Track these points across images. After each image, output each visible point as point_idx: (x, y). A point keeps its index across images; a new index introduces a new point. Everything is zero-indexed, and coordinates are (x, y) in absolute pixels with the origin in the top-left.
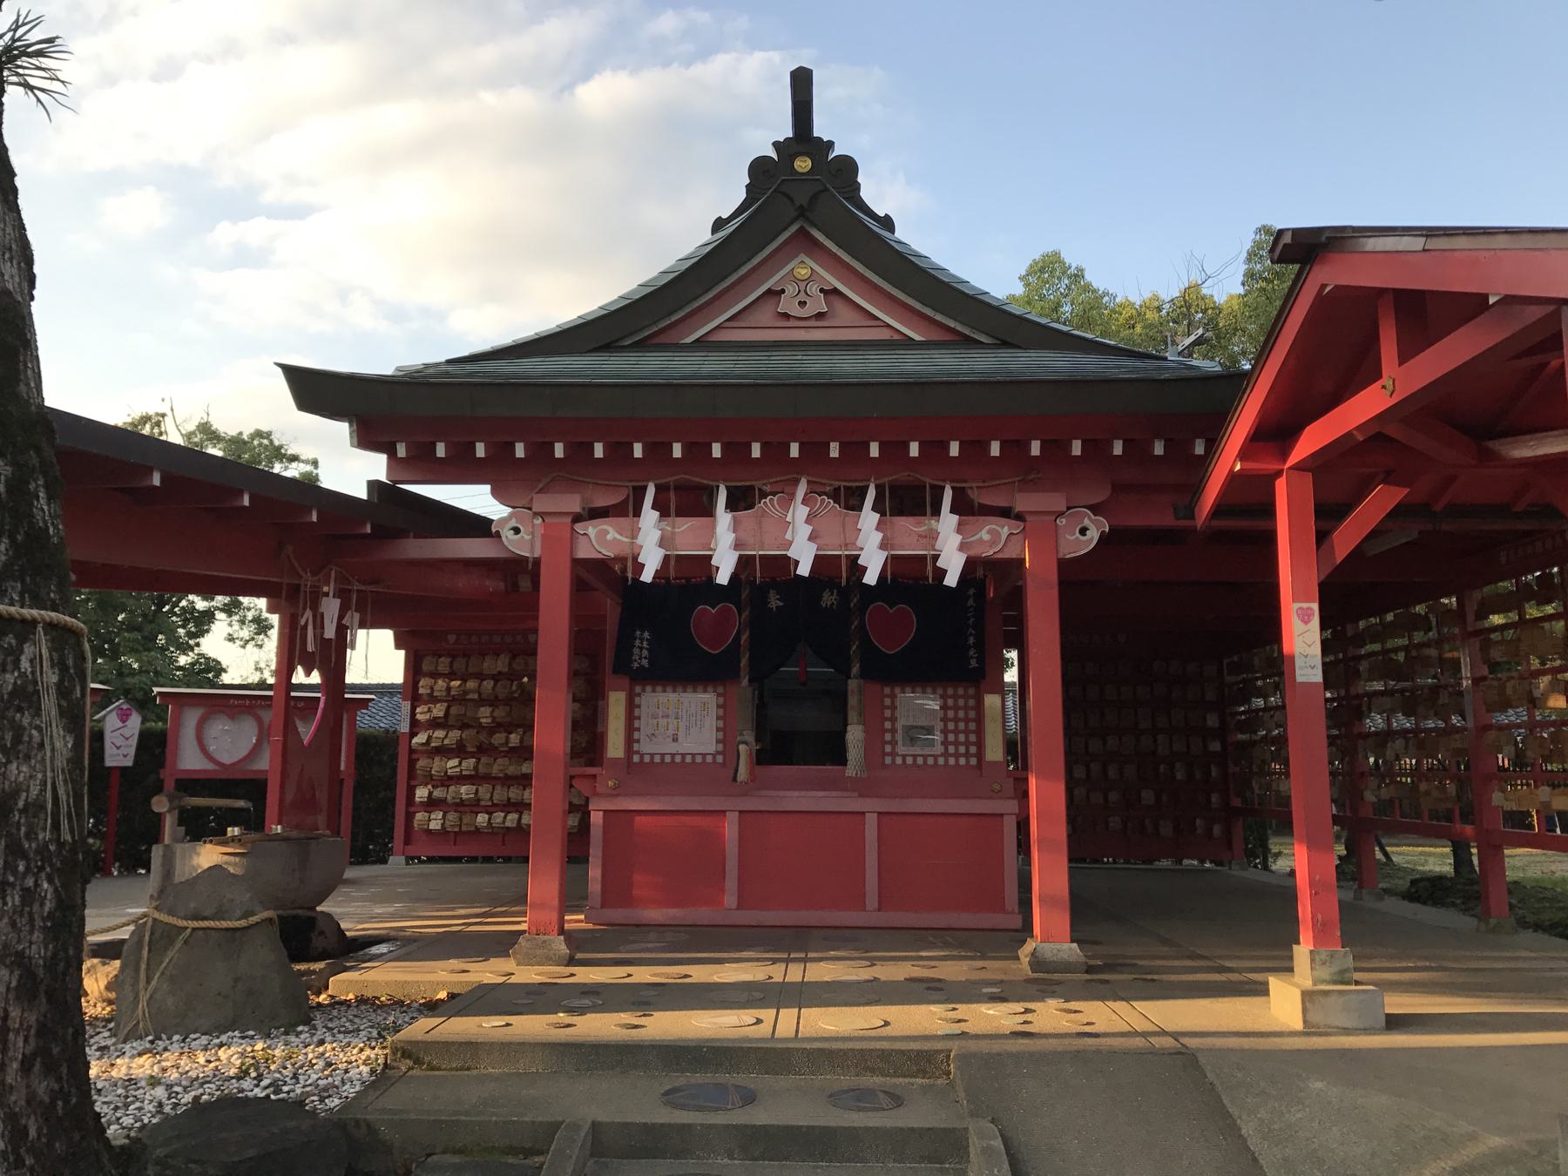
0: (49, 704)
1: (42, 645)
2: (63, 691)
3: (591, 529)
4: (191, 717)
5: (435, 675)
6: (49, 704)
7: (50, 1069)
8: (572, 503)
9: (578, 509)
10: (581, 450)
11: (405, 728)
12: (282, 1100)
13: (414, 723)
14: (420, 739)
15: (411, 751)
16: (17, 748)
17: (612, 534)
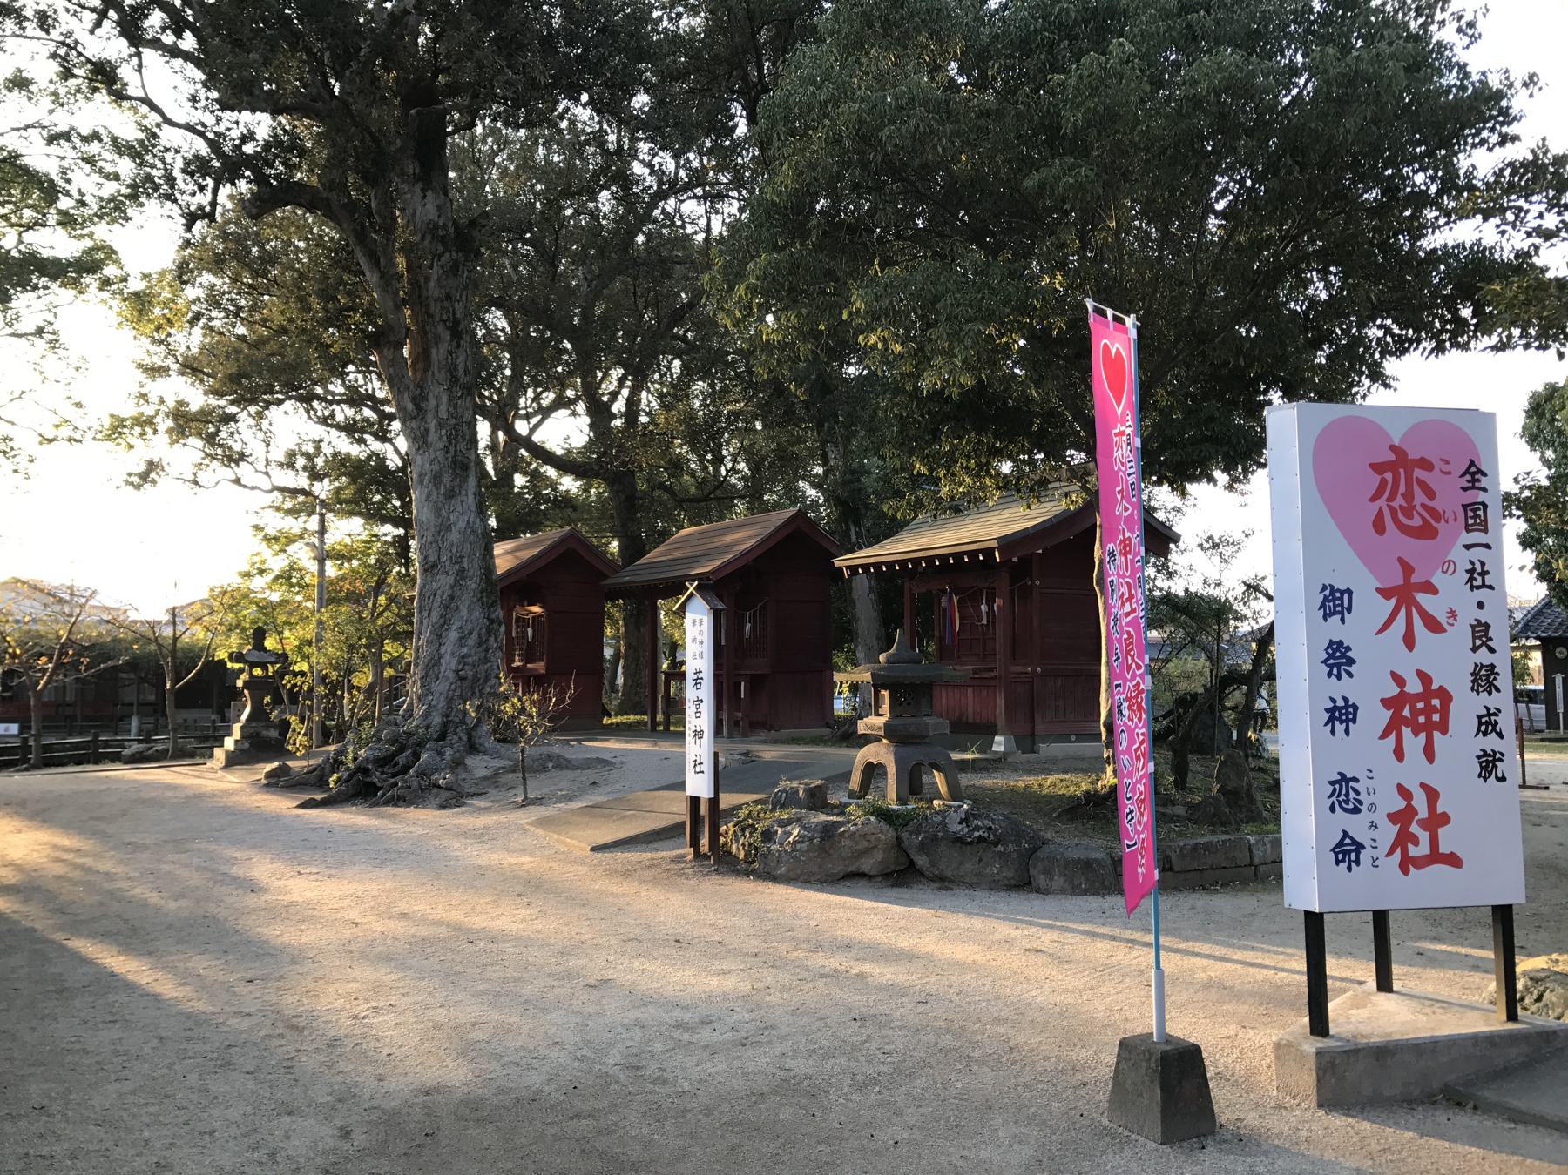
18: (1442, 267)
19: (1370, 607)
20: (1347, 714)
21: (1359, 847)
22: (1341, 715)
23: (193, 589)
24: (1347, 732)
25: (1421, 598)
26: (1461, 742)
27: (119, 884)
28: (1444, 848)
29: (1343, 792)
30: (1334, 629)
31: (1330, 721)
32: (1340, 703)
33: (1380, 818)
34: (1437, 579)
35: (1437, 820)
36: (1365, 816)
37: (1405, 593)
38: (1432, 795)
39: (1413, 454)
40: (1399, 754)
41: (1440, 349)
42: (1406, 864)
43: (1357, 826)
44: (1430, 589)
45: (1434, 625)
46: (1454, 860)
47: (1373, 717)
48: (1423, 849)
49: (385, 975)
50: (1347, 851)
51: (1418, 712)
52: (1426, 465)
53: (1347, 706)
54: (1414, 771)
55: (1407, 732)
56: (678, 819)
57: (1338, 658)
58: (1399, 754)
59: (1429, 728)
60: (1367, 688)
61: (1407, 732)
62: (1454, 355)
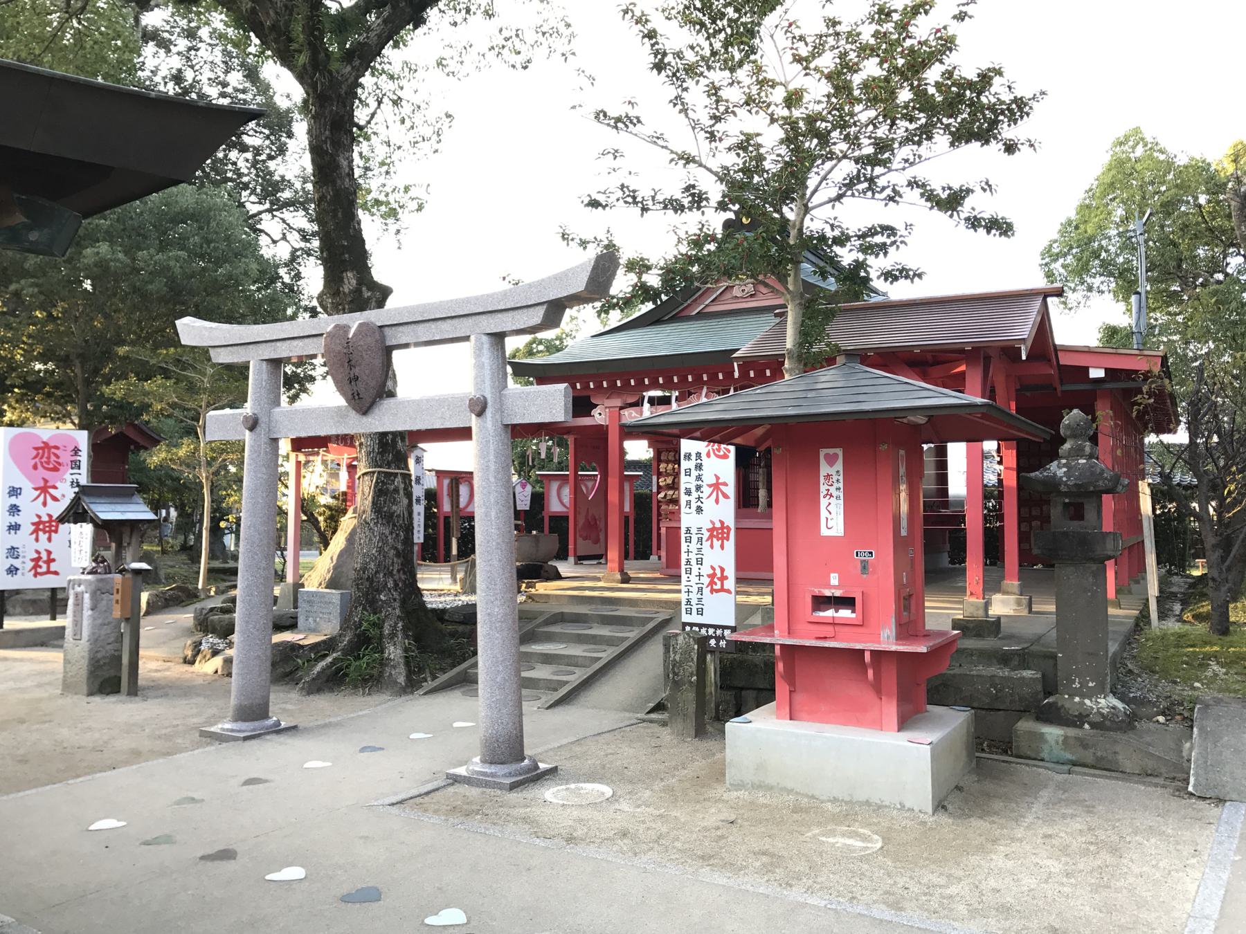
0: (401, 492)
1: (399, 479)
2: (405, 489)
3: (626, 412)
4: (554, 486)
5: (668, 462)
6: (401, 492)
7: (405, 573)
8: (618, 402)
9: (620, 405)
10: (612, 385)
11: (655, 490)
12: (62, 435)
13: (659, 487)
14: (662, 495)
15: (659, 502)
16: (395, 502)
17: (634, 414)
19: (29, 492)
20: (723, 533)
21: (17, 569)
24: (722, 547)
25: (52, 491)
28: (52, 569)
30: (13, 500)
31: (36, 531)
32: (718, 525)
33: (27, 560)
34: (58, 484)
35: (50, 561)
36: (21, 559)
37: (44, 488)
38: (49, 553)
39: (52, 444)
40: (37, 540)
42: (36, 575)
43: (17, 563)
44: (55, 487)
46: (56, 573)
47: (27, 528)
48: (44, 569)
52: (57, 448)
53: (723, 527)
54: (43, 544)
55: (41, 533)
56: (149, 618)
58: (37, 540)
59: (722, 539)
61: (41, 533)
62: (1059, 227)
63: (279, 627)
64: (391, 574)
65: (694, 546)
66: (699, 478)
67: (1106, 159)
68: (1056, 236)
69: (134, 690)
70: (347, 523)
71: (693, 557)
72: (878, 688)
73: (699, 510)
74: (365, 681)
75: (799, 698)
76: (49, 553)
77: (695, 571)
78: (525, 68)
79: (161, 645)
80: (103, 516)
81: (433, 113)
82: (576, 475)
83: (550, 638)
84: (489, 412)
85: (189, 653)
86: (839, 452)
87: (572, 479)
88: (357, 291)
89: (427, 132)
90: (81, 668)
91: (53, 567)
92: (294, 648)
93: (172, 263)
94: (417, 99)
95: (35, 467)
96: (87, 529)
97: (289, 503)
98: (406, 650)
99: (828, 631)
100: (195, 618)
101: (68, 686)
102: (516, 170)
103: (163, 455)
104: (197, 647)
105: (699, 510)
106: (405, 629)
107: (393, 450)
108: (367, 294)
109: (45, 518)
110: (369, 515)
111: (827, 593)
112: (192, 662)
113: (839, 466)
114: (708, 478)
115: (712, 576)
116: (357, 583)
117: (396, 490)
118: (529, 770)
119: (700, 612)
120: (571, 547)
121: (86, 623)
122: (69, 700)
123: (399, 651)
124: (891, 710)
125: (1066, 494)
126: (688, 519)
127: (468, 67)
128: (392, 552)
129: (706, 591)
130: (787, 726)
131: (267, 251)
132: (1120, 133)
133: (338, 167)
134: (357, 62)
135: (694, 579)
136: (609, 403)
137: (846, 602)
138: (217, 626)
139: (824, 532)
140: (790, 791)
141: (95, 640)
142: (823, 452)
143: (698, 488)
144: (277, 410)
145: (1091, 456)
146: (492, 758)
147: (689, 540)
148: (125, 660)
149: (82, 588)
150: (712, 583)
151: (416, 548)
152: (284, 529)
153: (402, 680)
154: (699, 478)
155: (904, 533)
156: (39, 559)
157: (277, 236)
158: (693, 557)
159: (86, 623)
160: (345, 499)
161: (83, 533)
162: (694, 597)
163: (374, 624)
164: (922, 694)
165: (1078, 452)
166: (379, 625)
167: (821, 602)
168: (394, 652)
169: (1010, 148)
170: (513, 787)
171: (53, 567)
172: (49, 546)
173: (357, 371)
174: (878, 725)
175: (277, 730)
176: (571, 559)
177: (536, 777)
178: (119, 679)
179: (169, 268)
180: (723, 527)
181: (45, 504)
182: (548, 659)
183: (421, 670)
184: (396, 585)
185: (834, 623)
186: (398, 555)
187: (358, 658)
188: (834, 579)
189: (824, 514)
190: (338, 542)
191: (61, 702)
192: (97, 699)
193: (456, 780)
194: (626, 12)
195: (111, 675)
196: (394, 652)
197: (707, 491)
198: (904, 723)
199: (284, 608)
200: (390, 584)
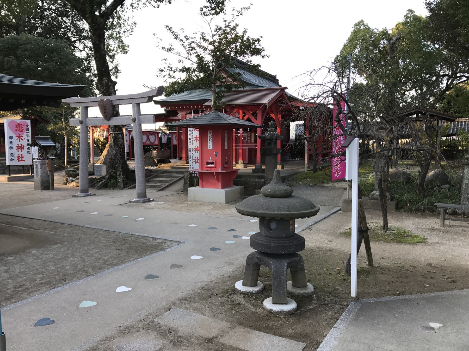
1: (120, 135)
8: (185, 113)
18: (252, 49)
19: (15, 138)
22: (11, 148)
23: (350, 34)
26: (25, 150)
27: (183, 205)
29: (12, 155)
30: (11, 140)
31: (18, 149)
35: (22, 157)
37: (19, 137)
41: (344, 45)
43: (13, 158)
45: (22, 140)
46: (24, 161)
47: (15, 148)
48: (21, 159)
49: (345, 264)
50: (12, 160)
51: (21, 148)
53: (22, 146)
54: (20, 152)
57: (11, 143)
60: (15, 145)
63: (90, 175)
64: (119, 160)
65: (191, 152)
66: (192, 136)
67: (352, 30)
68: (339, 54)
69: (53, 189)
70: (107, 146)
71: (191, 155)
72: (217, 179)
73: (193, 144)
74: (112, 187)
75: (204, 183)
76: (22, 155)
77: (192, 157)
78: (158, 7)
79: (58, 177)
80: (42, 145)
81: (130, 22)
82: (179, 132)
83: (162, 177)
84: (136, 121)
85: (65, 182)
86: (212, 131)
87: (177, 133)
88: (107, 83)
89: (128, 28)
90: (39, 183)
91: (23, 159)
92: (94, 179)
93: (50, 67)
94: (125, 18)
95: (16, 131)
96: (37, 148)
97: (91, 141)
98: (123, 179)
99: (209, 169)
100: (66, 173)
101: (35, 188)
102: (149, 55)
103: (52, 127)
104: (67, 180)
105: (193, 144)
106: (123, 174)
107: (118, 129)
108: (110, 84)
109: (20, 145)
110: (112, 145)
111: (209, 161)
112: (66, 184)
113: (212, 134)
114: (195, 136)
115: (195, 159)
116: (110, 162)
117: (119, 138)
118: (147, 199)
119: (193, 168)
120: (177, 154)
121: (39, 172)
122: (37, 192)
123: (121, 179)
124: (220, 184)
125: (268, 140)
126: (190, 146)
127: (141, 6)
128: (119, 154)
129: (194, 163)
130: (201, 189)
131: (78, 54)
132: (357, 22)
133: (101, 48)
134: (105, 18)
135: (191, 160)
136: (182, 113)
137: (212, 163)
138: (73, 175)
139: (209, 148)
140: (200, 201)
141: (42, 176)
142: (209, 131)
143: (192, 138)
144: (87, 119)
145: (274, 131)
146: (139, 197)
147: (190, 151)
148: (50, 181)
149: (38, 163)
150: (195, 161)
151: (126, 154)
152: (90, 149)
153: (122, 186)
154: (192, 136)
155: (226, 148)
156: (19, 157)
157: (82, 49)
158: (191, 155)
159: (39, 172)
160: (107, 139)
161: (35, 150)
162: (191, 164)
163: (114, 173)
164: (232, 182)
165: (271, 131)
166: (116, 173)
167: (208, 163)
168: (120, 179)
169: (263, 57)
170: (143, 202)
171: (23, 159)
172: (22, 153)
173: (106, 111)
174: (218, 188)
175: (91, 195)
176: (178, 158)
177: (149, 201)
178: (49, 186)
179: (49, 68)
180: (22, 146)
181: (20, 141)
182: (160, 181)
183: (127, 184)
184: (120, 163)
185: (210, 167)
186: (120, 155)
187: (111, 181)
188: (211, 159)
189: (209, 144)
190: (105, 152)
191: (35, 191)
192: (44, 191)
193: (131, 202)
194: (167, 27)
195: (47, 185)
196: (120, 179)
197: (194, 139)
198: (223, 187)
199: (91, 170)
200: (119, 163)
